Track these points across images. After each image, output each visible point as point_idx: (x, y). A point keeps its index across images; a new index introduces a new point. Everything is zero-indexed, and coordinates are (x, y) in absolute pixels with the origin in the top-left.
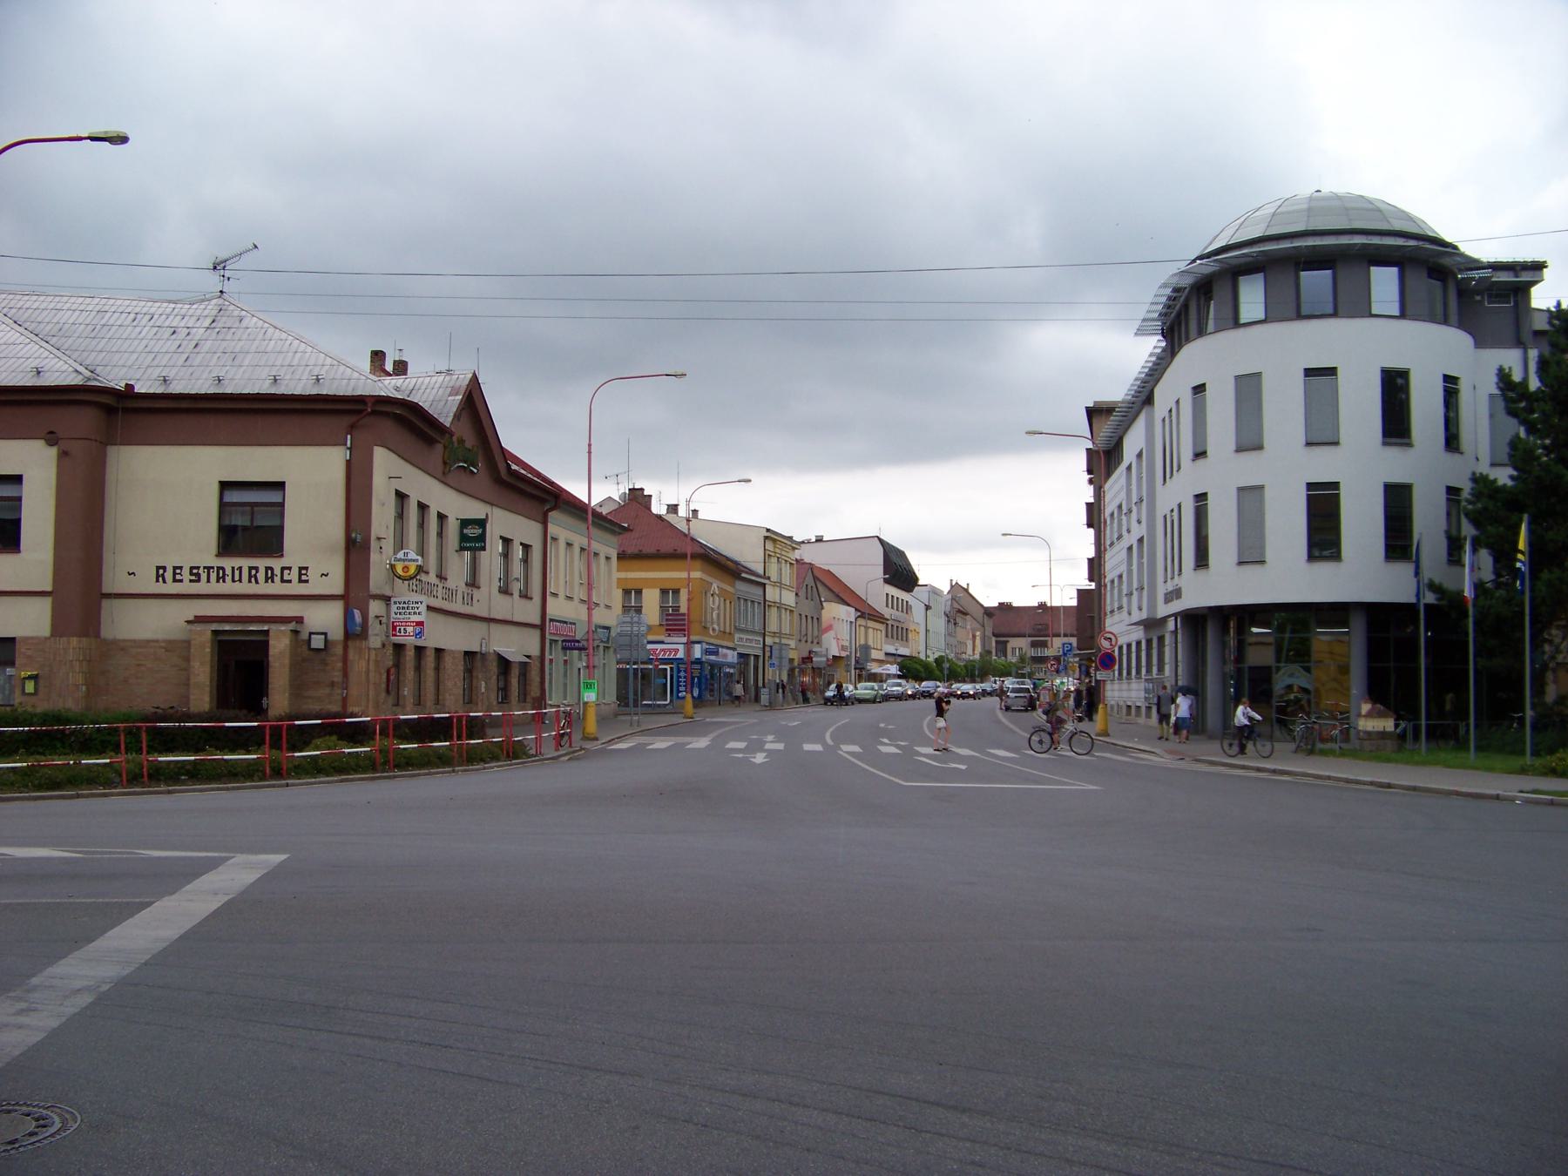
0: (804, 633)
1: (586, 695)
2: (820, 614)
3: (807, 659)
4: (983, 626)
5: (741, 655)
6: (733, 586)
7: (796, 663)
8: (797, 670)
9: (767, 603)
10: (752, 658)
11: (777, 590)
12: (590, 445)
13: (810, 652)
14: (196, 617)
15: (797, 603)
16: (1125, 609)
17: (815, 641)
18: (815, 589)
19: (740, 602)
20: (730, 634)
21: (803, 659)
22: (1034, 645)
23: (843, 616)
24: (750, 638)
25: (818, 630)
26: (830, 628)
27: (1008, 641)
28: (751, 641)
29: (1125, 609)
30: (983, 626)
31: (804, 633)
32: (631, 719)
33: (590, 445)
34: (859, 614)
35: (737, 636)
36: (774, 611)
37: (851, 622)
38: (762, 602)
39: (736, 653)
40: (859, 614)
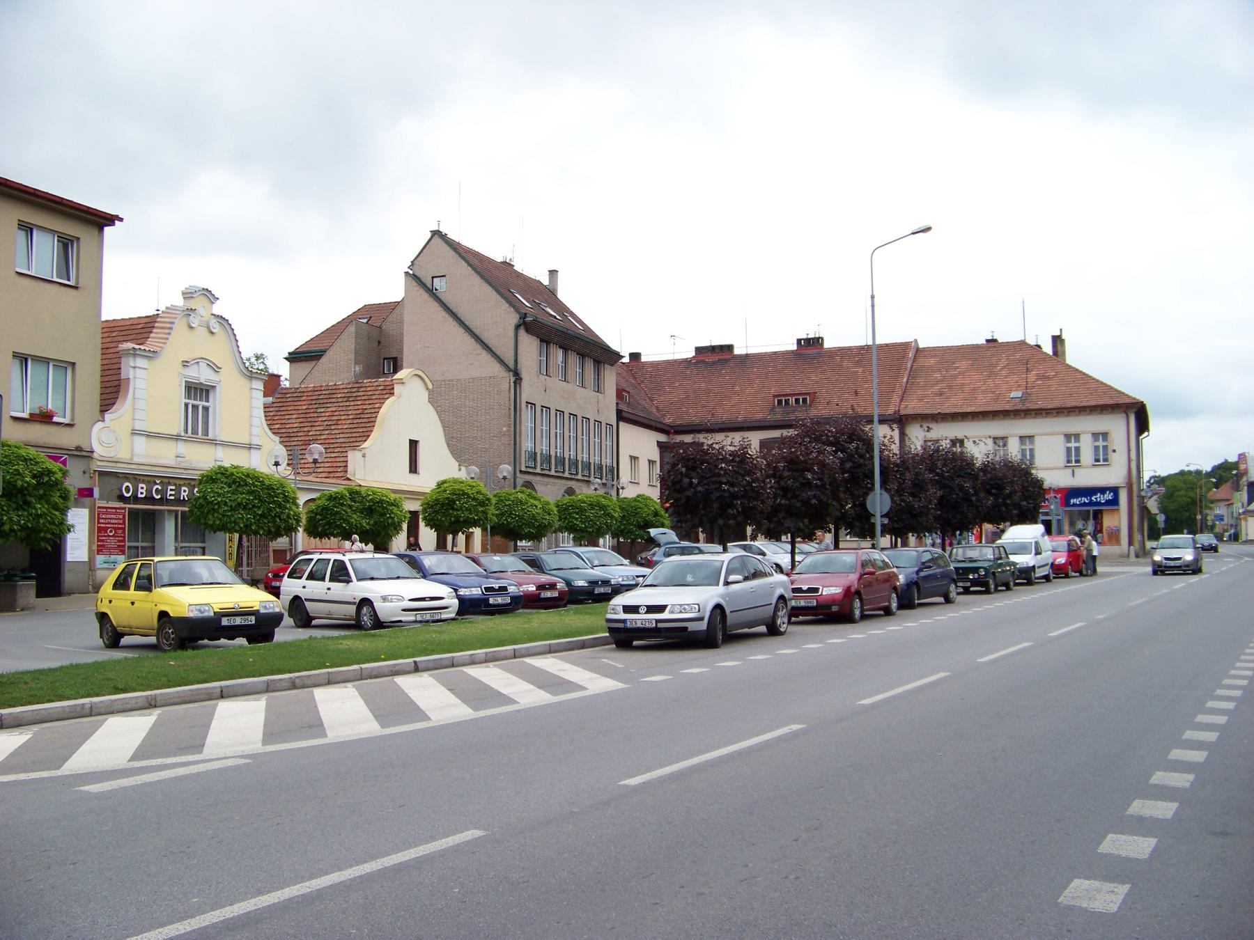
12: (873, 297)
33: (873, 297)
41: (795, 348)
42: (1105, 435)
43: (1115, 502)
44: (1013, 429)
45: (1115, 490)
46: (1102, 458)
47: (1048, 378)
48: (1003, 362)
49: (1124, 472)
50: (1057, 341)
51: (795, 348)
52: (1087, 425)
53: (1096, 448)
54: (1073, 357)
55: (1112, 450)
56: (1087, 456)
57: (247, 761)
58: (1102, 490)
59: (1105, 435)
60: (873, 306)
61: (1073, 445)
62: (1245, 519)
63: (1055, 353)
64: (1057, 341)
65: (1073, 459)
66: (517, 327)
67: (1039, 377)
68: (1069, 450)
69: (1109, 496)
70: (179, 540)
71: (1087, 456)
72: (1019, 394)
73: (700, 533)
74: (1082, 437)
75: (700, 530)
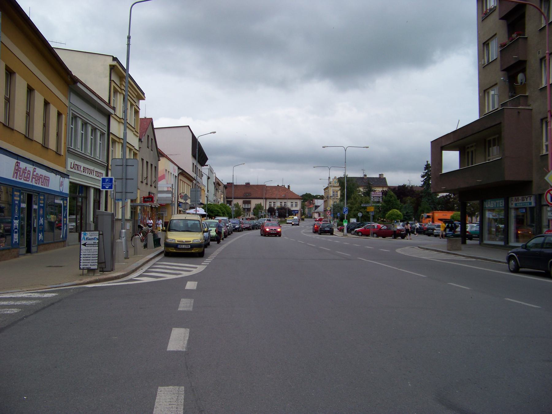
0: (145, 176)
1: (25, 206)
2: (157, 164)
3: (149, 198)
4: (223, 193)
5: (74, 187)
6: (68, 98)
7: (138, 201)
8: (139, 208)
9: (111, 136)
10: (92, 191)
11: (122, 127)
12: (129, 38)
13: (149, 193)
14: (227, 183)
15: (140, 148)
16: (85, 172)
17: (153, 185)
18: (154, 140)
19: (76, 122)
20: (58, 153)
21: (144, 198)
22: (244, 203)
23: (171, 171)
24: (92, 168)
25: (155, 177)
26: (163, 177)
27: (232, 201)
28: (91, 172)
29: (85, 172)
30: (223, 193)
31: (145, 176)
32: (54, 240)
33: (129, 38)
34: (181, 171)
35: (70, 161)
36: (118, 147)
37: (176, 176)
38: (106, 133)
39: (66, 182)
40: (181, 171)
41: (245, 184)
42: (297, 203)
43: (298, 212)
44: (283, 201)
45: (298, 211)
46: (296, 206)
47: (288, 193)
48: (281, 190)
49: (299, 208)
50: (289, 186)
51: (245, 184)
52: (294, 201)
53: (295, 204)
54: (291, 189)
55: (270, 201)
56: (294, 205)
57: (54, 294)
58: (296, 211)
59: (297, 203)
60: (129, 45)
61: (292, 204)
62: (314, 214)
63: (288, 188)
64: (289, 186)
65: (292, 206)
66: (224, 187)
67: (287, 193)
68: (291, 204)
69: (297, 212)
70: (178, 213)
71: (294, 205)
72: (284, 195)
73: (430, 164)
74: (272, 203)
75: (430, 165)
